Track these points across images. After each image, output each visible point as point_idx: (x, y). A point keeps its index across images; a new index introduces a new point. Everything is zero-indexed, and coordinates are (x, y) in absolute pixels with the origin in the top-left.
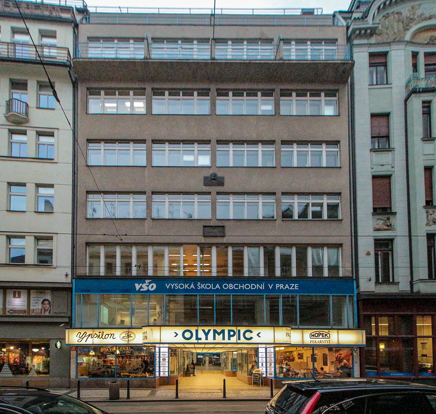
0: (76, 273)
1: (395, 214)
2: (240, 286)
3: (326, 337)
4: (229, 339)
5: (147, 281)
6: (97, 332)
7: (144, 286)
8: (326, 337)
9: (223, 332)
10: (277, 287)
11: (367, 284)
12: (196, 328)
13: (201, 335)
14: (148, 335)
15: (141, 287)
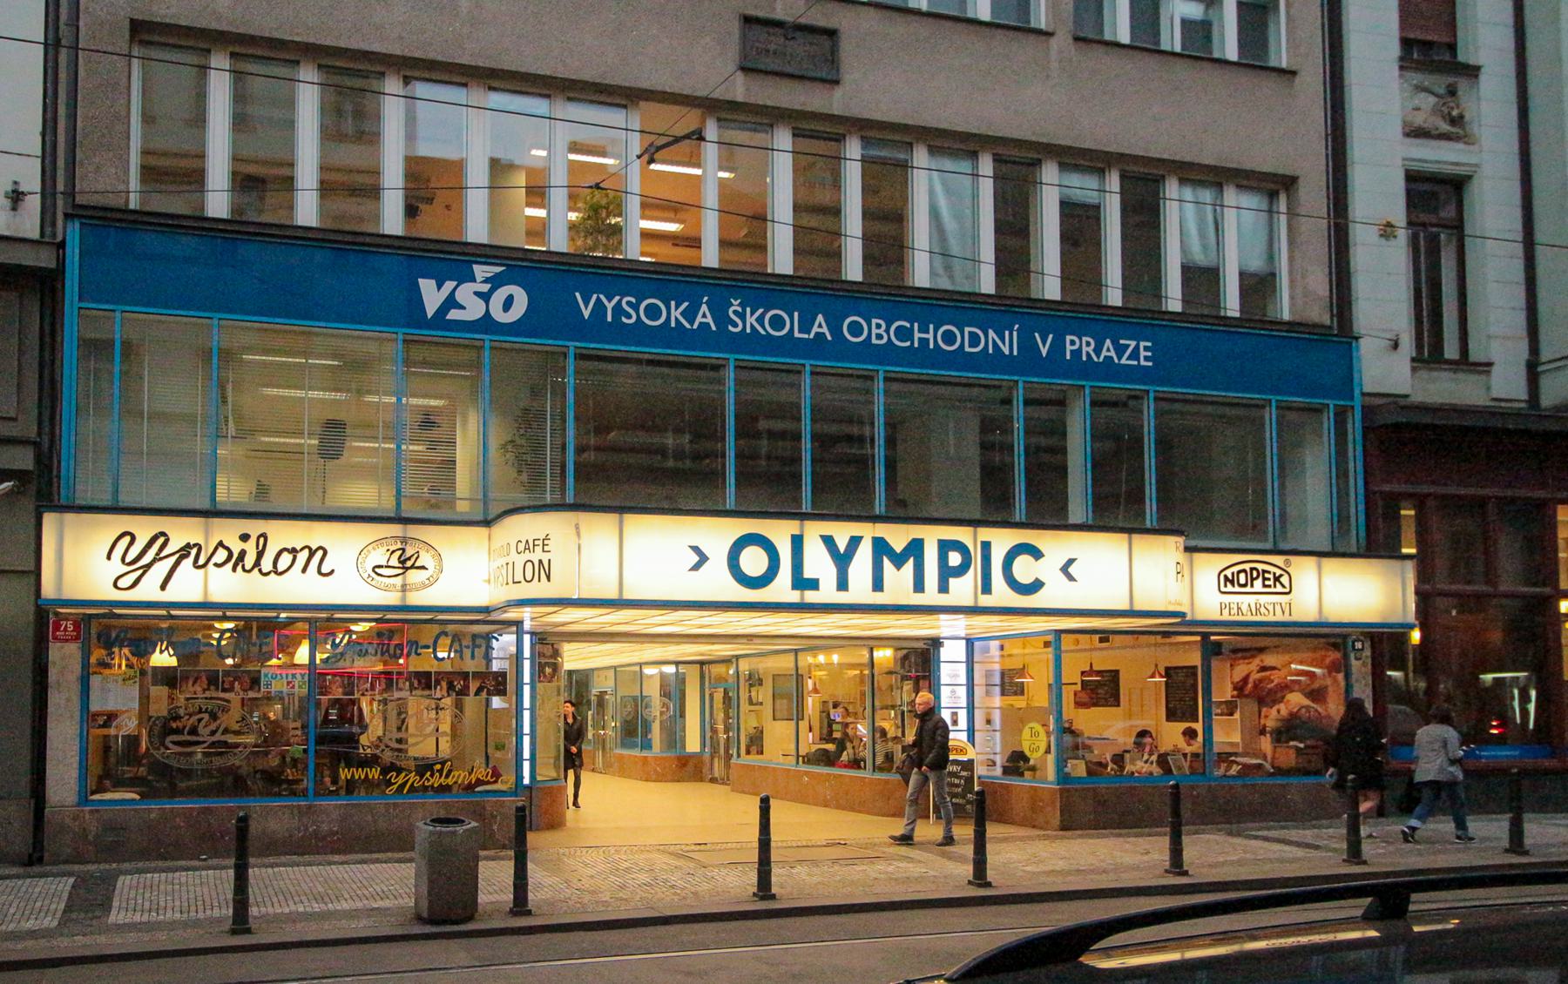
0: (71, 193)
1: (1472, 72)
2: (917, 335)
3: (1279, 588)
4: (943, 588)
5: (481, 271)
6: (229, 532)
7: (465, 293)
8: (1279, 588)
9: (915, 548)
10: (1069, 348)
11: (1384, 367)
12: (792, 527)
13: (818, 563)
14: (560, 555)
15: (451, 302)
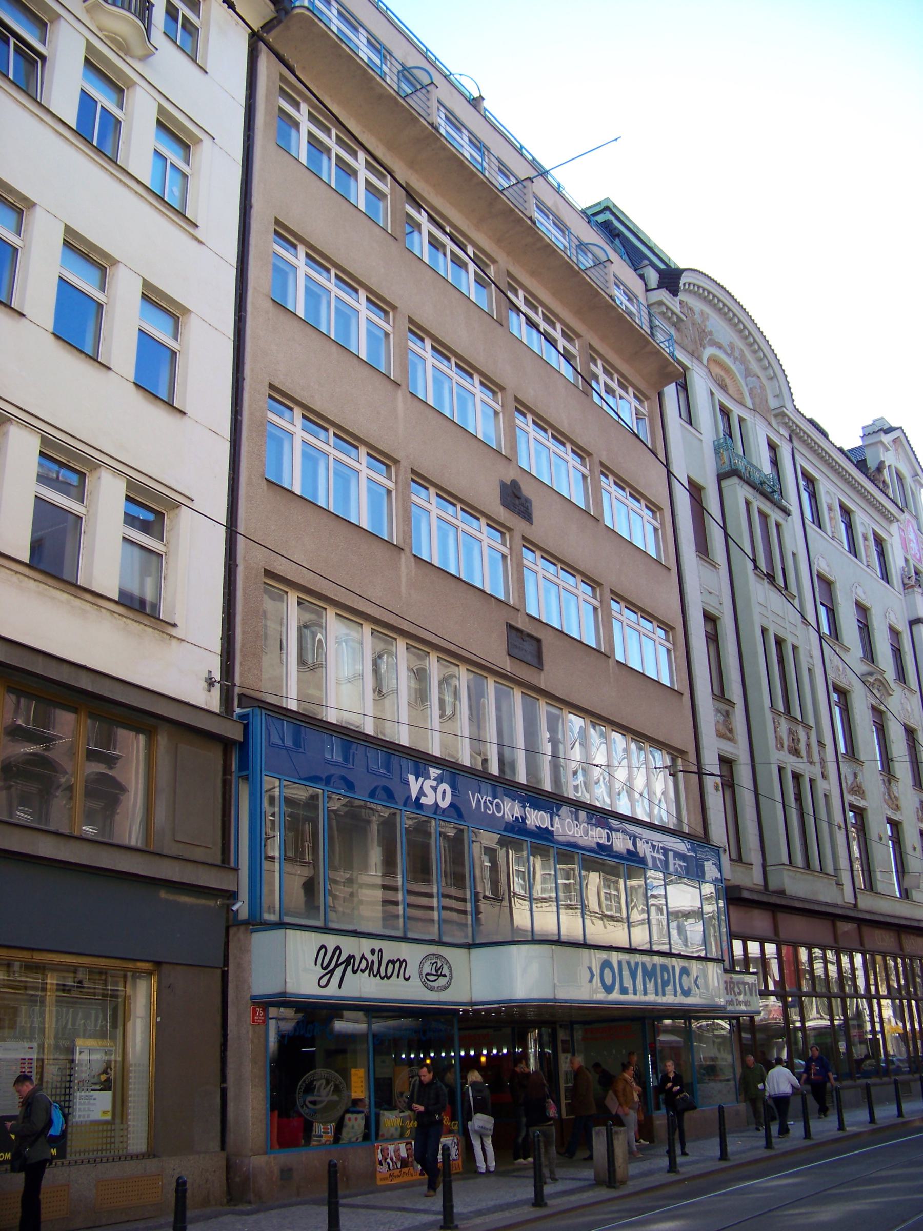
5: (434, 772)
